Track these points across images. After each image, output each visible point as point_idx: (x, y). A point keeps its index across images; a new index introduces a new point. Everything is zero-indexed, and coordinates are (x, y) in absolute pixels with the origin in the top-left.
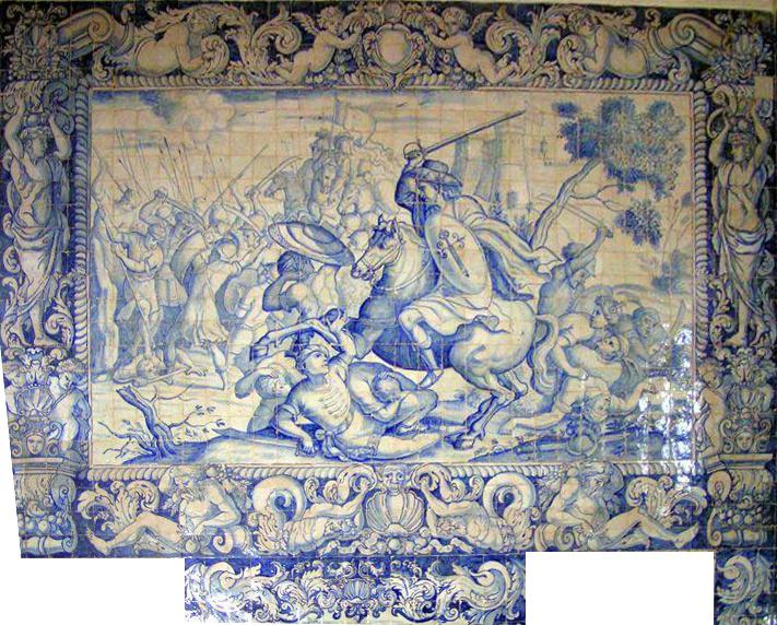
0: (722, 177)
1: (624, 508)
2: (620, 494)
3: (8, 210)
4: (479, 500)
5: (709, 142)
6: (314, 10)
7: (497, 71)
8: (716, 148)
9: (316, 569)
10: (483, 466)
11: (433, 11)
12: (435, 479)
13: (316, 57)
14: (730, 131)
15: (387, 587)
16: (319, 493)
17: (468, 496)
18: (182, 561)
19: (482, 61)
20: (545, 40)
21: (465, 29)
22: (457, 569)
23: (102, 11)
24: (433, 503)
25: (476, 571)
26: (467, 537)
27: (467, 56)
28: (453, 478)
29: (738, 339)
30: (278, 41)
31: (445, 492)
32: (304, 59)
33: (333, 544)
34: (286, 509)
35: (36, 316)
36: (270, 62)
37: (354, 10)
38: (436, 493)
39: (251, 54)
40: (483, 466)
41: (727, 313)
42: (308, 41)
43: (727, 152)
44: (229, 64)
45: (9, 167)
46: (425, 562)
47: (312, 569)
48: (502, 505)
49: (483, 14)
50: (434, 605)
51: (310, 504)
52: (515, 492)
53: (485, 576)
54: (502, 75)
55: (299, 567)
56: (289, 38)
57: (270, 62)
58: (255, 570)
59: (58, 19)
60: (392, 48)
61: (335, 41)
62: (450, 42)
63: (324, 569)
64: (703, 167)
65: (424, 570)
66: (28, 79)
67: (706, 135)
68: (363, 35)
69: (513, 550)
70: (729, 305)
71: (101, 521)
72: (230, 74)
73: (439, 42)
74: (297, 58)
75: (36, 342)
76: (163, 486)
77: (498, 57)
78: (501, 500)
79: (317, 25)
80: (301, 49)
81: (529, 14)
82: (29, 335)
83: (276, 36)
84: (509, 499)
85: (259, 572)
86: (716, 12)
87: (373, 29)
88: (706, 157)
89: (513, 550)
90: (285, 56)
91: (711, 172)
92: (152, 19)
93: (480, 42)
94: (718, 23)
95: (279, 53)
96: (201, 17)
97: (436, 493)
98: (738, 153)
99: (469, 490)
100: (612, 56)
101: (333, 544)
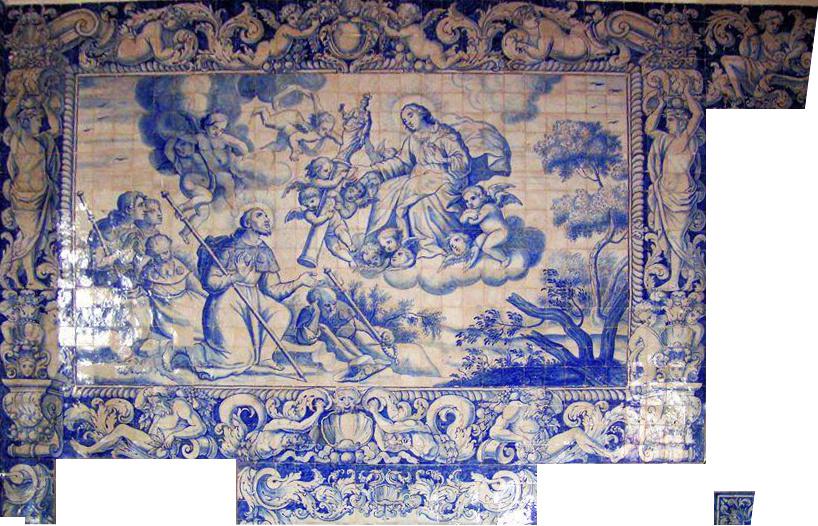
0: (655, 148)
1: (564, 428)
2: (559, 417)
3: (9, 177)
4: (424, 420)
5: (644, 118)
6: (276, 9)
7: (446, 58)
8: (652, 120)
9: (350, 476)
10: (471, 391)
11: (388, 6)
12: (383, 403)
13: (278, 44)
14: (665, 108)
15: (412, 492)
16: (279, 410)
17: (414, 417)
18: (233, 462)
19: (430, 49)
20: (491, 32)
21: (417, 22)
22: (474, 476)
23: (89, 11)
24: (381, 422)
25: (490, 478)
26: (412, 450)
27: (421, 46)
28: (402, 400)
29: (672, 285)
30: (243, 33)
31: (391, 412)
32: (265, 50)
33: (288, 454)
34: (249, 419)
35: (28, 263)
36: (235, 51)
37: (311, 7)
38: (384, 413)
39: (218, 44)
40: (471, 391)
41: (660, 262)
42: (269, 33)
43: (662, 125)
44: (198, 53)
45: (9, 142)
46: (445, 470)
47: (346, 476)
48: (443, 424)
49: (435, 10)
50: (454, 507)
51: (269, 419)
52: (457, 414)
53: (499, 483)
54: (450, 61)
55: (334, 475)
56: (254, 32)
57: (235, 51)
58: (298, 476)
59: (50, 19)
60: (348, 35)
61: (296, 34)
62: (403, 33)
63: (357, 476)
64: (640, 138)
65: (447, 477)
66: (26, 67)
67: (642, 111)
68: (320, 27)
69: (456, 462)
70: (662, 255)
71: (82, 432)
72: (198, 62)
73: (392, 32)
74: (260, 47)
75: (28, 286)
76: (139, 402)
77: (446, 47)
78: (444, 420)
79: (279, 20)
80: (263, 39)
81: (477, 10)
82: (23, 279)
83: (241, 29)
84: (451, 418)
85: (299, 478)
86: (650, 6)
87: (329, 22)
88: (643, 131)
89: (456, 462)
90: (249, 46)
91: (647, 142)
92: (130, 17)
93: (431, 34)
94: (650, 16)
95: (243, 43)
96: (171, 15)
97: (384, 413)
98: (672, 126)
99: (414, 411)
100: (261, 44)
101: (288, 454)
